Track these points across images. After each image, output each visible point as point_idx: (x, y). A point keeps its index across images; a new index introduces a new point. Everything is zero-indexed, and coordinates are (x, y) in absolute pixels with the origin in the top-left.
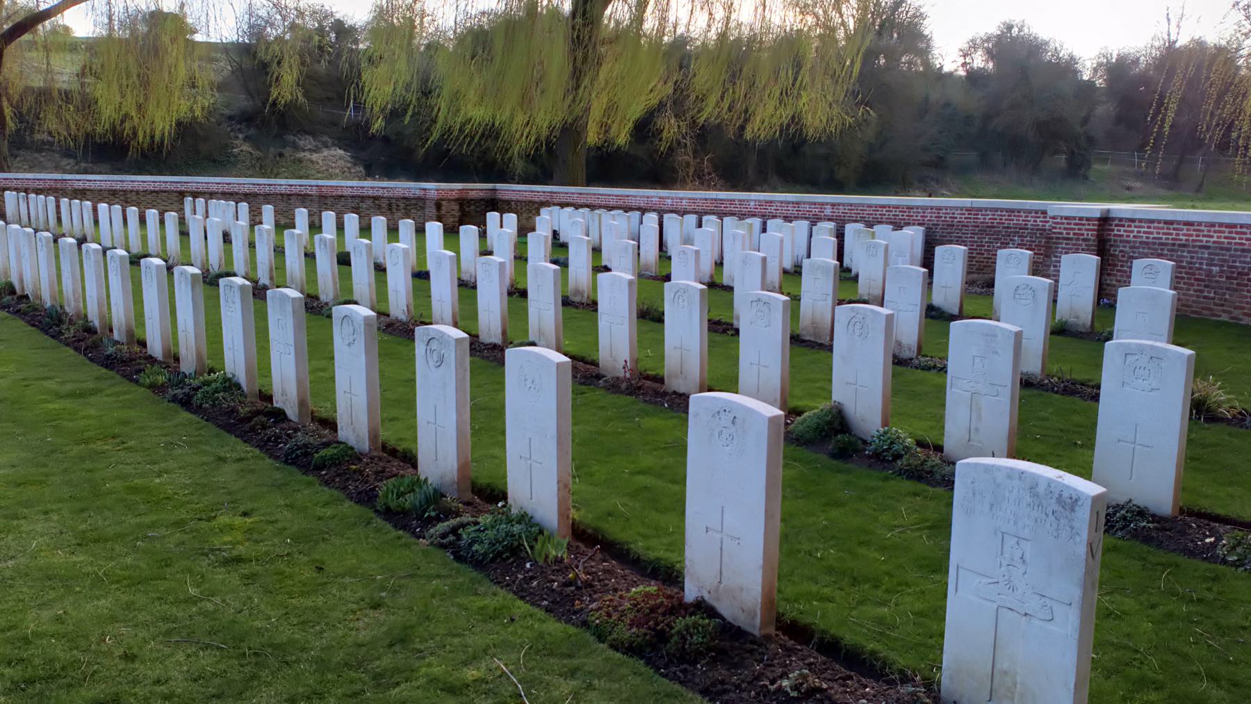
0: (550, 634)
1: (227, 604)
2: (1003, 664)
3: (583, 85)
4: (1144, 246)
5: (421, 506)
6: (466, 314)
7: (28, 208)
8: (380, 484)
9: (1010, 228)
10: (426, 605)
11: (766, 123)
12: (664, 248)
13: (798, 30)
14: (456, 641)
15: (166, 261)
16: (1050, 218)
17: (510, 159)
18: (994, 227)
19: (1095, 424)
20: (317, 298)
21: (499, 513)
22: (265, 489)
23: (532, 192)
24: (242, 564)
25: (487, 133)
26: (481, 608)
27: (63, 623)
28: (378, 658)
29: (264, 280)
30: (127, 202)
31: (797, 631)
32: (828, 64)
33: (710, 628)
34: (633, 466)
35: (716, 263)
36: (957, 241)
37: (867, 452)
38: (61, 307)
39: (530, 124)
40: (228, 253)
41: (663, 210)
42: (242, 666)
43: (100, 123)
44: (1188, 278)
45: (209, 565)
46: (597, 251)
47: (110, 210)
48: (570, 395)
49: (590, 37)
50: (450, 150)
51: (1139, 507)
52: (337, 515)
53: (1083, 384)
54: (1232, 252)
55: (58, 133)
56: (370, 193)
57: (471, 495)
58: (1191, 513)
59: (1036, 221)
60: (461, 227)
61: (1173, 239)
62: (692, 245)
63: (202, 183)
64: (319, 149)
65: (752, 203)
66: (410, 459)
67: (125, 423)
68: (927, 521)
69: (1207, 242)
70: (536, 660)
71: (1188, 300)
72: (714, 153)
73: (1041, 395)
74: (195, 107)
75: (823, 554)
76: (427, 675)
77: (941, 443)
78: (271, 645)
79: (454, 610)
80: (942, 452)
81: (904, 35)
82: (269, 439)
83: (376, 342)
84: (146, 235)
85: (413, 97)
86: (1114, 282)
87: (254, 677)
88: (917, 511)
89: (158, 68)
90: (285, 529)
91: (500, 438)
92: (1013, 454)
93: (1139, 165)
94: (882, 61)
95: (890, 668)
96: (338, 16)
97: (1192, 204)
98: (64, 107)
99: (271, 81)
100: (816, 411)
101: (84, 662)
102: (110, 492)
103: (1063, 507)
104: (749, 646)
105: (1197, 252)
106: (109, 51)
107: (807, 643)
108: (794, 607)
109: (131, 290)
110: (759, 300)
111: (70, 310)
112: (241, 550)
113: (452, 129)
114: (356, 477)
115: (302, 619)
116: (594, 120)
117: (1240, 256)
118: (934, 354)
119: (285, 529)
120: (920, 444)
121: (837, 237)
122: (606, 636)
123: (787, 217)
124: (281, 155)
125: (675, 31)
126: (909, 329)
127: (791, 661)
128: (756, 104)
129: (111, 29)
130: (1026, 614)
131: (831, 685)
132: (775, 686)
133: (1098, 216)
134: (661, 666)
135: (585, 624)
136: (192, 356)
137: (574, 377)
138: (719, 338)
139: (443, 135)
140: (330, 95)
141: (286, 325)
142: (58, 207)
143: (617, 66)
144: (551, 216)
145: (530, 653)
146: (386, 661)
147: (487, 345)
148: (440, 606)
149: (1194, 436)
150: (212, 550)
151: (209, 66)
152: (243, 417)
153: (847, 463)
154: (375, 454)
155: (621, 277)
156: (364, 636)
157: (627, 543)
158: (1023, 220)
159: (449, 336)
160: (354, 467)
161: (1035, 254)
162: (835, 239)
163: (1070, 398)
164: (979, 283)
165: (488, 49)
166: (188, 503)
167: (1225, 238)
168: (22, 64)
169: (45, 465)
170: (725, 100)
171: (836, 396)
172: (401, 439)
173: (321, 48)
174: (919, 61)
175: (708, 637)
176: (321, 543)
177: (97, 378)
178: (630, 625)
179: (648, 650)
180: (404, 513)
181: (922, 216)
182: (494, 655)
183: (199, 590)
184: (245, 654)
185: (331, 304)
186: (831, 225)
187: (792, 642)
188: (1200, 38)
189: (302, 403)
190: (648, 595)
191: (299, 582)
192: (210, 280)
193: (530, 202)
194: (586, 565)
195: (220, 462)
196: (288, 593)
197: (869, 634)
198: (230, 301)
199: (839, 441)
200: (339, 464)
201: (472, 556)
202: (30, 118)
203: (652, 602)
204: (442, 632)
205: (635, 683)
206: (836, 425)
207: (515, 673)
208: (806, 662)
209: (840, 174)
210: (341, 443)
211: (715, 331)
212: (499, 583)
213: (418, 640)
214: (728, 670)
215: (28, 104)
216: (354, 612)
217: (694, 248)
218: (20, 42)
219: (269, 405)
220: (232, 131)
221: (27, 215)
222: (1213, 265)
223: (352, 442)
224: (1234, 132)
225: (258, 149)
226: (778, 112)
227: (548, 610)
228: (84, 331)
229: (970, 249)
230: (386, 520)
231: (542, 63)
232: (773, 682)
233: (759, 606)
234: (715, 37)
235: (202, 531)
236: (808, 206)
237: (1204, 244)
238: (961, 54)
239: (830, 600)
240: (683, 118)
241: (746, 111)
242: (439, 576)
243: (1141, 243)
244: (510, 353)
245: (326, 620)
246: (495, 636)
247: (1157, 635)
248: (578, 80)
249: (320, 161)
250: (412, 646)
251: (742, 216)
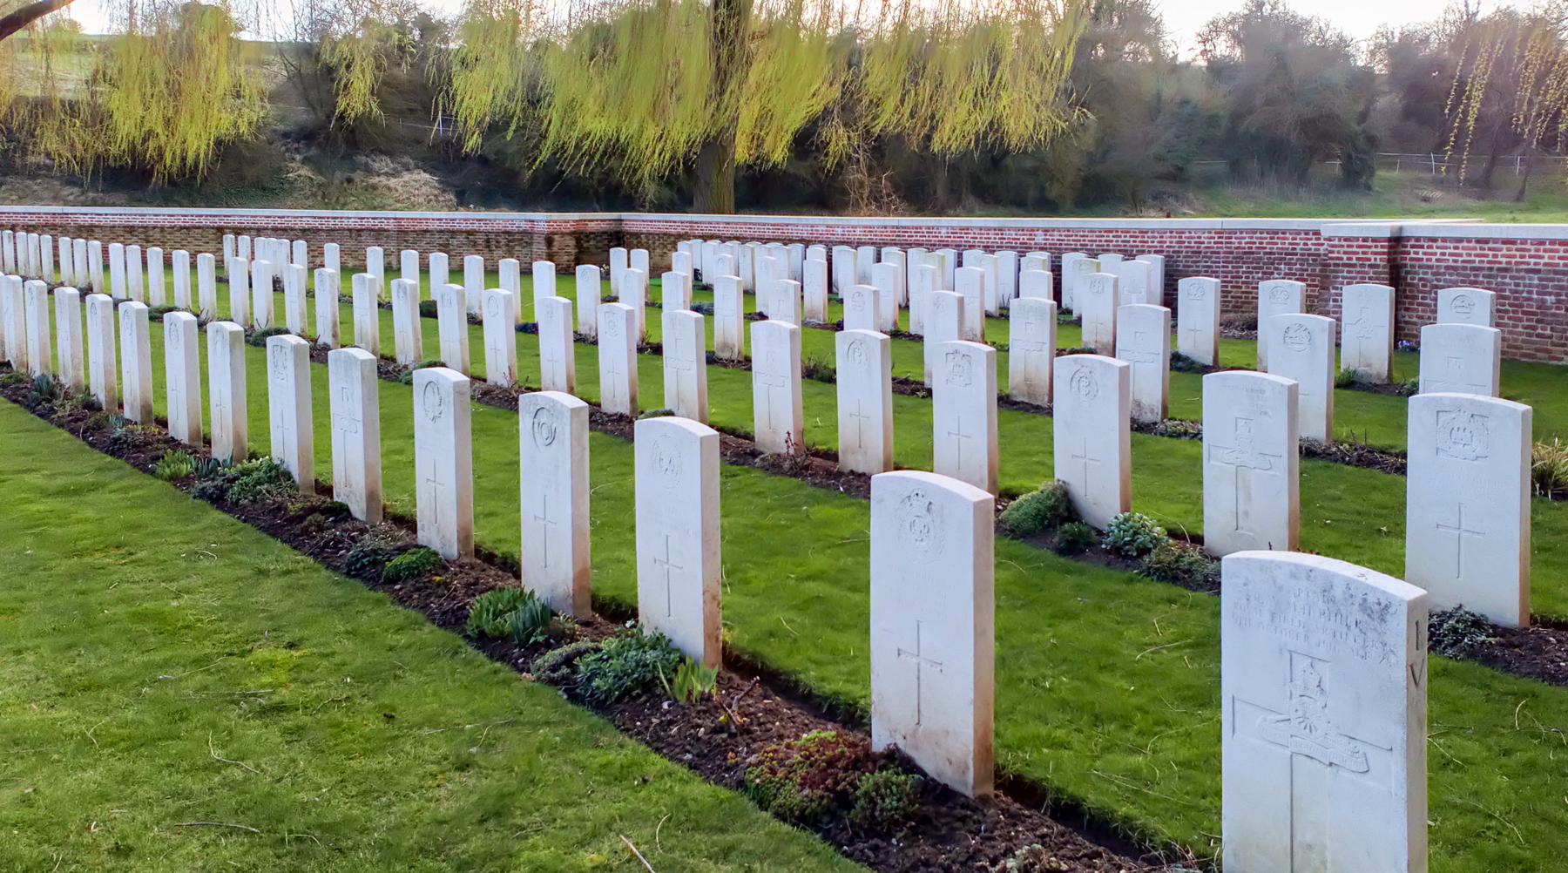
0: (695, 800)
1: (262, 771)
2: (1305, 835)
3: (729, 90)
4: (1451, 271)
5: (525, 628)
6: (584, 379)
7: (15, 250)
8: (471, 600)
9: (1274, 254)
10: (530, 764)
11: (957, 132)
12: (834, 289)
13: (993, 17)
14: (570, 812)
15: (198, 316)
16: (1325, 239)
17: (640, 181)
18: (1253, 253)
19: (1405, 504)
20: (393, 360)
21: (627, 636)
22: (319, 611)
23: (666, 222)
24: (285, 714)
25: (610, 150)
26: (604, 766)
27: (31, 806)
28: (465, 840)
29: (325, 338)
30: (148, 242)
31: (1023, 790)
32: (1033, 57)
33: (908, 788)
34: (800, 569)
35: (900, 306)
36: (1206, 272)
37: (1103, 546)
38: (54, 377)
39: (664, 139)
40: (279, 307)
41: (832, 242)
42: (279, 857)
43: (115, 142)
44: (1514, 312)
45: (240, 717)
46: (749, 294)
47: (125, 251)
48: (718, 479)
49: (737, 31)
50: (564, 172)
51: (1473, 615)
52: (414, 643)
53: (1383, 452)
55: (59, 155)
56: (463, 226)
57: (591, 613)
58: (1546, 623)
59: (1306, 244)
60: (577, 268)
61: (1489, 262)
62: (869, 284)
63: (247, 216)
64: (397, 172)
65: (944, 231)
66: (511, 567)
67: (134, 527)
68: (1188, 636)
69: (1535, 264)
70: (677, 837)
71: (1516, 340)
72: (893, 170)
73: (1328, 467)
74: (239, 122)
75: (1052, 683)
76: (530, 862)
77: (1200, 532)
78: (320, 826)
79: (568, 769)
80: (1202, 544)
81: (1126, 19)
82: (326, 545)
83: (469, 414)
84: (172, 283)
85: (517, 108)
86: (1415, 319)
88: (1173, 623)
89: (192, 73)
90: (344, 664)
91: (629, 536)
92: (1297, 545)
93: (1438, 169)
94: (1101, 52)
95: (1151, 841)
96: (422, 9)
97: (1511, 216)
98: (67, 122)
99: (338, 89)
100: (1035, 493)
101: (57, 860)
102: (109, 621)
103: (1369, 615)
104: (959, 812)
105: (1523, 278)
106: (129, 52)
107: (1038, 806)
108: (1017, 756)
109: (149, 353)
111: (66, 380)
112: (284, 695)
113: (566, 146)
114: (440, 592)
115: (363, 787)
116: (744, 132)
118: (1183, 417)
119: (344, 664)
120: (1173, 534)
121: (1053, 271)
122: (770, 801)
123: (988, 247)
124: (350, 181)
125: (841, 22)
126: (1151, 387)
127: (1017, 832)
128: (945, 109)
129: (132, 25)
130: (1331, 764)
131: (1073, 866)
132: (998, 868)
133: (1388, 235)
134: (843, 841)
135: (741, 784)
136: (228, 436)
137: (723, 454)
138: (907, 401)
139: (555, 153)
140: (413, 105)
141: (352, 395)
142: (56, 248)
143: (771, 65)
144: (691, 252)
145: (668, 827)
146: (476, 844)
147: (611, 416)
148: (549, 763)
149: (1540, 518)
150: (245, 696)
151: (258, 71)
152: (292, 517)
153: (1078, 561)
154: (466, 560)
155: (779, 326)
156: (446, 809)
157: (796, 672)
158: (1290, 244)
159: (562, 405)
160: (438, 578)
161: (1308, 285)
162: (1051, 273)
163: (1366, 471)
164: (1237, 324)
165: (610, 47)
166: (215, 632)
167: (1560, 258)
168: (12, 68)
169: (22, 587)
170: (906, 104)
171: (1060, 474)
172: (500, 541)
173: (401, 48)
174: (1147, 50)
175: (905, 799)
176: (392, 681)
177: (99, 469)
178: (801, 785)
179: (826, 819)
180: (504, 638)
181: (1159, 242)
182: (621, 831)
183: (225, 752)
184: (283, 839)
185: (410, 367)
186: (1045, 255)
187: (1017, 805)
188: (1508, 7)
189: (372, 497)
190: (824, 743)
191: (361, 736)
192: (256, 339)
193: (665, 234)
194: (741, 703)
195: (261, 576)
196: (346, 752)
197: (1120, 793)
198: (280, 364)
199: (1066, 532)
200: (419, 575)
201: (592, 695)
202: (22, 136)
203: (829, 753)
204: (551, 800)
205: (809, 867)
206: (1062, 510)
207: (649, 856)
208: (1038, 833)
209: (1054, 192)
210: (422, 547)
211: (902, 393)
212: (627, 730)
213: (518, 812)
214: (933, 845)
215: (20, 118)
216: (434, 776)
217: (873, 288)
218: (11, 40)
219: (328, 500)
220: (287, 150)
221: (13, 259)
222: (1545, 294)
223: (436, 545)
224: (1561, 123)
225: (321, 174)
226: (972, 118)
227: (692, 766)
228: (84, 408)
229: (1223, 282)
230: (479, 648)
231: (677, 63)
232: (994, 862)
233: (972, 756)
234: (891, 28)
235: (232, 670)
236: (1014, 233)
237: (1532, 266)
238: (1200, 39)
239: (1064, 746)
240: (854, 127)
241: (933, 117)
242: (547, 723)
243: (1447, 268)
244: (640, 425)
245: (396, 789)
246: (622, 804)
247: (1516, 793)
248: (722, 83)
249: (399, 188)
250: (511, 821)
251: (931, 247)
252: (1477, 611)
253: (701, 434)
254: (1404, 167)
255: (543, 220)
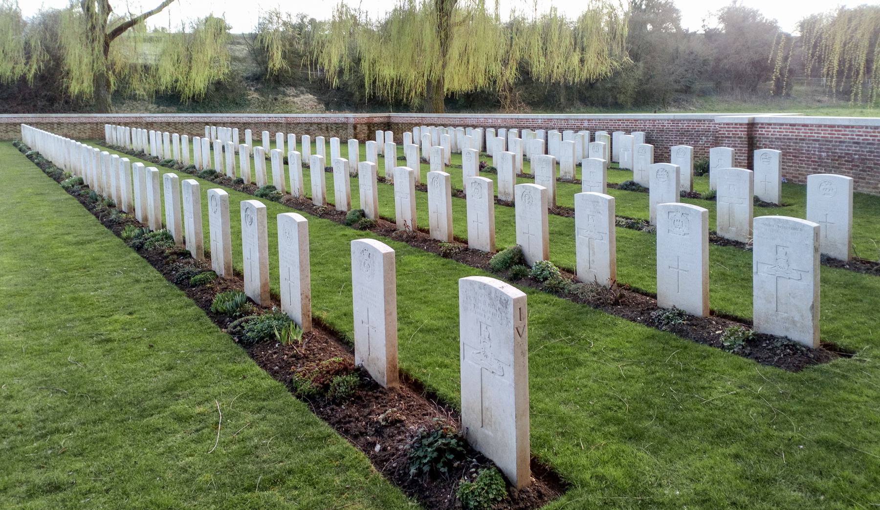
2: (486, 404)
44: (807, 161)
54: (834, 143)
56: (316, 121)
87: (72, 409)
105: (811, 144)
110: (476, 182)
117: (839, 146)
124: (276, 99)
133: (747, 122)
167: (829, 134)
171: (518, 242)
209: (621, 98)
225: (263, 96)
237: (816, 138)
252: (681, 308)
253: (298, 221)
254: (809, 84)
255: (350, 116)
